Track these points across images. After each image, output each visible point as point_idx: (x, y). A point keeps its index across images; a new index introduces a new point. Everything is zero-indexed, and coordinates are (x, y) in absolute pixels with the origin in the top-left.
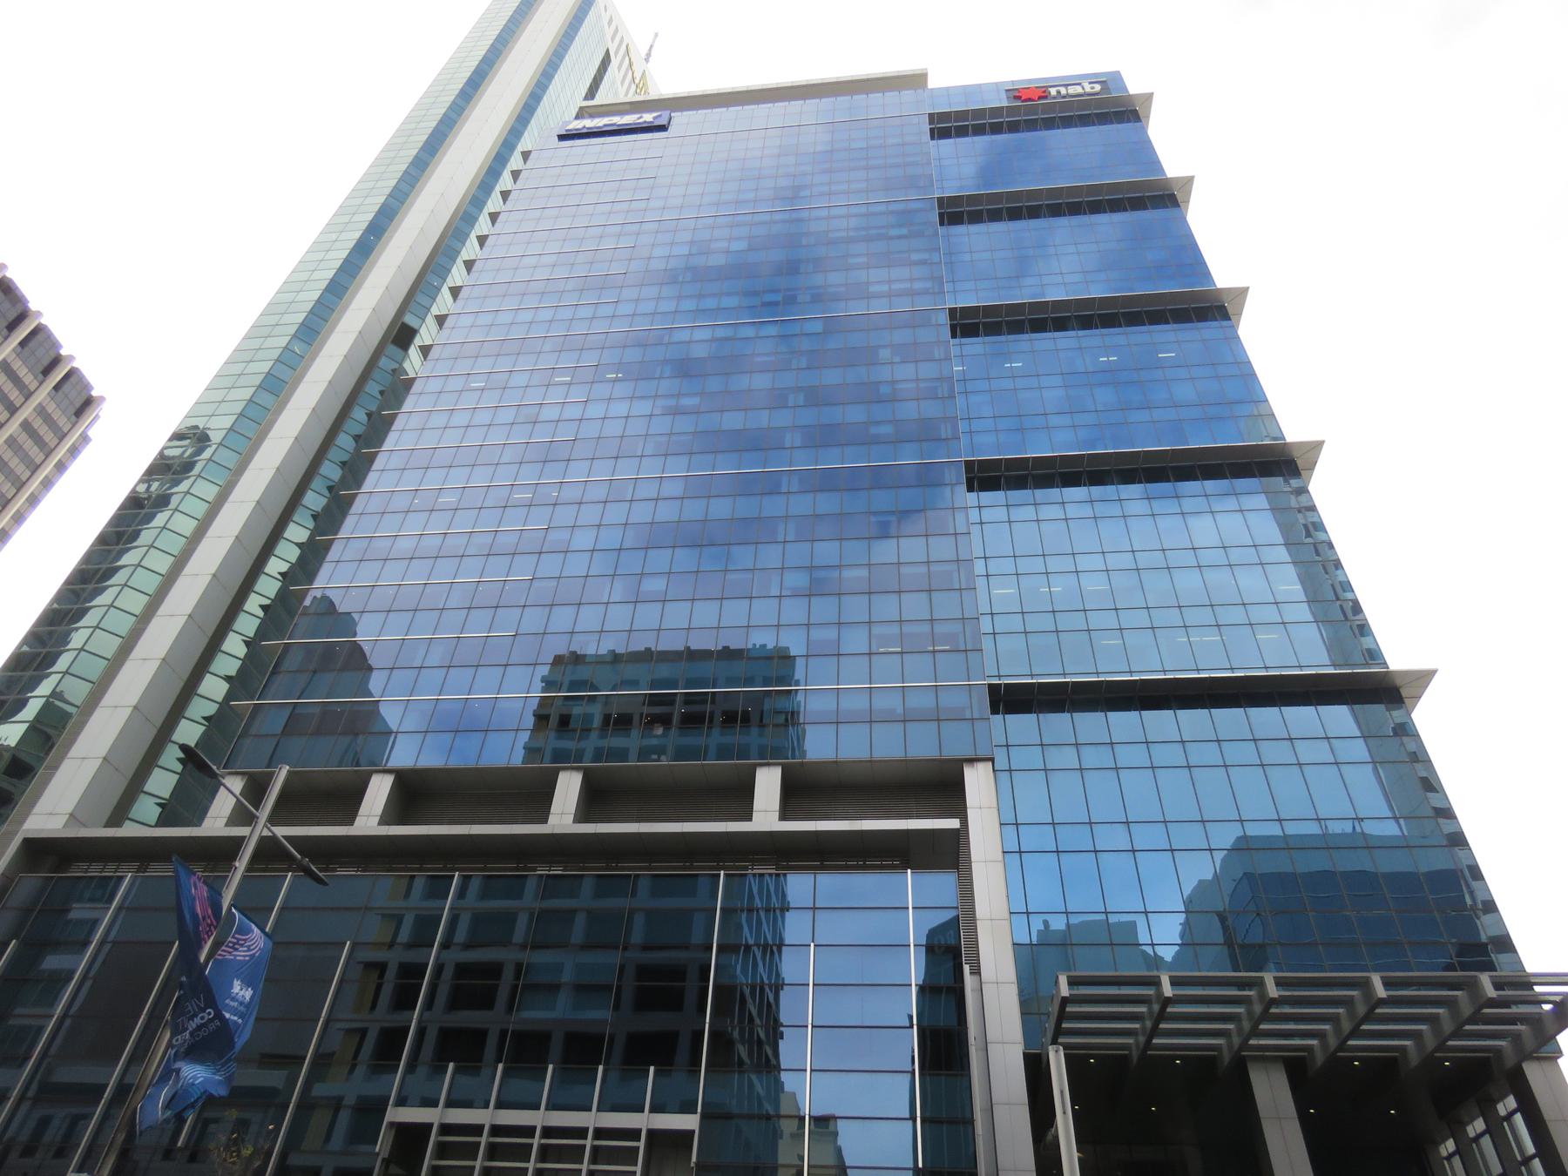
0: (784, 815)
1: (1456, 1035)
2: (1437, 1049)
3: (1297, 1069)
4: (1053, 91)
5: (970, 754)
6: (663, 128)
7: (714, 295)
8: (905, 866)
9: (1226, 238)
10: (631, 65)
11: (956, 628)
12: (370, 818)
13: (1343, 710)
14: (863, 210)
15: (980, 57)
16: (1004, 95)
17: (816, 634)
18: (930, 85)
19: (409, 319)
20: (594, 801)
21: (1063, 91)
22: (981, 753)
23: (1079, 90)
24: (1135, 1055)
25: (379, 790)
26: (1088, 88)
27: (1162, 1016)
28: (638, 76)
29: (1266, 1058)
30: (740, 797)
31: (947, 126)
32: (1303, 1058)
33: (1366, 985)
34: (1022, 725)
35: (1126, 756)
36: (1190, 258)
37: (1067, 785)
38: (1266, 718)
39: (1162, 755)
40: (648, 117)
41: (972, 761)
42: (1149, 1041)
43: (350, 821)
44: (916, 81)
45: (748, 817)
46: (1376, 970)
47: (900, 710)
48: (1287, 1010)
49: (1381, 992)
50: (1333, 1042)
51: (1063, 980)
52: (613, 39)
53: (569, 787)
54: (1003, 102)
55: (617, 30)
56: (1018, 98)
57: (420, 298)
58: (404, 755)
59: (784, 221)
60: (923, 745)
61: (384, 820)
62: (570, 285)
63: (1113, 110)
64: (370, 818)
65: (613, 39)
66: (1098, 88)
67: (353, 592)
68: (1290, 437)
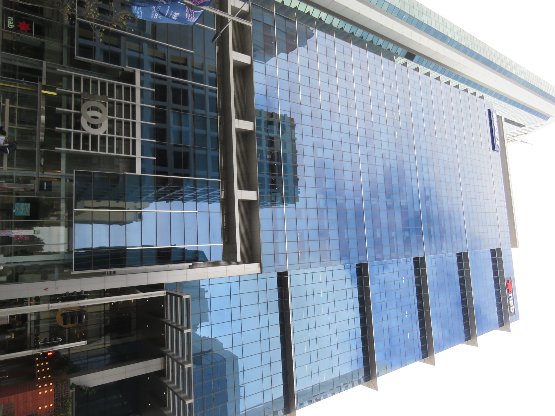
1: (174, 393)
3: (162, 373)
4: (511, 295)
6: (494, 148)
10: (520, 135)
12: (235, 56)
18: (513, 250)
20: (244, 135)
21: (511, 299)
22: (263, 269)
23: (512, 304)
24: (165, 351)
25: (245, 59)
26: (512, 308)
27: (177, 329)
28: (515, 138)
29: (165, 363)
30: (246, 185)
31: (496, 256)
33: (189, 397)
34: (274, 283)
35: (264, 319)
37: (256, 348)
39: (264, 331)
40: (498, 143)
41: (261, 266)
43: (235, 49)
44: (514, 243)
47: (277, 241)
48: (181, 371)
52: (530, 128)
53: (248, 126)
54: (506, 276)
55: (533, 129)
58: (257, 67)
60: (266, 249)
61: (232, 6)
63: (504, 317)
64: (235, 56)
65: (530, 128)
66: (513, 311)
67: (315, 45)
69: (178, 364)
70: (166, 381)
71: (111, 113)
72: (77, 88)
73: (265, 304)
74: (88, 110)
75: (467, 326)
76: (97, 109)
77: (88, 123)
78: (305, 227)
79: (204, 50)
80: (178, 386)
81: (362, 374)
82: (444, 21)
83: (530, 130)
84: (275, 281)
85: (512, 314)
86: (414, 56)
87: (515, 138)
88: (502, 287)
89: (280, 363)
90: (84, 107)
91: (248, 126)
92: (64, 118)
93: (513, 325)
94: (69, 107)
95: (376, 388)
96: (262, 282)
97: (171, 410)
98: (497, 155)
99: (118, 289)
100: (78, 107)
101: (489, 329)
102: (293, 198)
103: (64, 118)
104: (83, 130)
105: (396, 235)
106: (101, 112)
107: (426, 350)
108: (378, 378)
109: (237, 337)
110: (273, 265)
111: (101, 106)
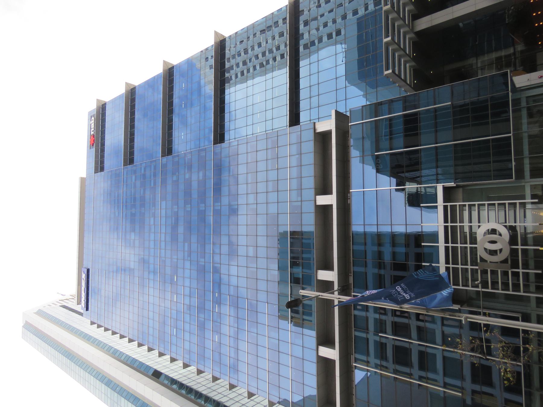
0: (331, 193)
1: (404, 50)
2: (410, 57)
3: (415, 17)
4: (92, 133)
5: (312, 131)
6: (88, 271)
7: (149, 234)
8: (349, 192)
9: (145, 71)
11: (270, 141)
13: (302, 63)
14: (124, 220)
15: (77, 159)
16: (92, 150)
17: (270, 189)
18: (85, 176)
19: (151, 372)
20: (328, 267)
21: (92, 130)
22: (312, 127)
23: (93, 125)
26: (93, 121)
28: (71, 297)
31: (100, 166)
32: (413, 70)
33: (387, 44)
34: (304, 116)
36: (150, 84)
37: (324, 99)
38: (303, 94)
40: (84, 276)
41: (315, 129)
42: (411, 299)
45: (334, 361)
46: (383, 73)
47: (297, 156)
48: (397, 68)
49: (389, 39)
50: (408, 58)
51: (386, 73)
52: (56, 305)
54: (94, 150)
56: (93, 145)
57: (142, 369)
59: (126, 219)
60: (309, 147)
61: (335, 349)
62: (141, 298)
63: (101, 113)
65: (56, 305)
66: (93, 118)
67: (250, 373)
68: (212, 43)
69: (399, 44)
70: (413, 64)
71: (474, 251)
72: (516, 275)
73: (312, 95)
74: (501, 250)
75: (133, 100)
76: (493, 253)
77: (500, 235)
78: (270, 173)
79: (368, 389)
80: (400, 57)
81: (227, 44)
82: (88, 163)
83: (56, 303)
84: (302, 119)
85: (94, 116)
86: (153, 375)
87: (71, 297)
88: (98, 141)
89: (301, 98)
90: (506, 253)
91: (324, 275)
92: (532, 263)
93: (93, 106)
94: (525, 251)
95: (216, 33)
96: (314, 116)
97: (406, 9)
98: (88, 264)
99: (462, 2)
100: (514, 252)
101: (114, 101)
102: (282, 236)
103: (532, 263)
104: (505, 226)
105: (185, 175)
106: (485, 249)
107: (170, 74)
108: (213, 43)
109: (341, 96)
110: (302, 155)
111: (486, 256)
